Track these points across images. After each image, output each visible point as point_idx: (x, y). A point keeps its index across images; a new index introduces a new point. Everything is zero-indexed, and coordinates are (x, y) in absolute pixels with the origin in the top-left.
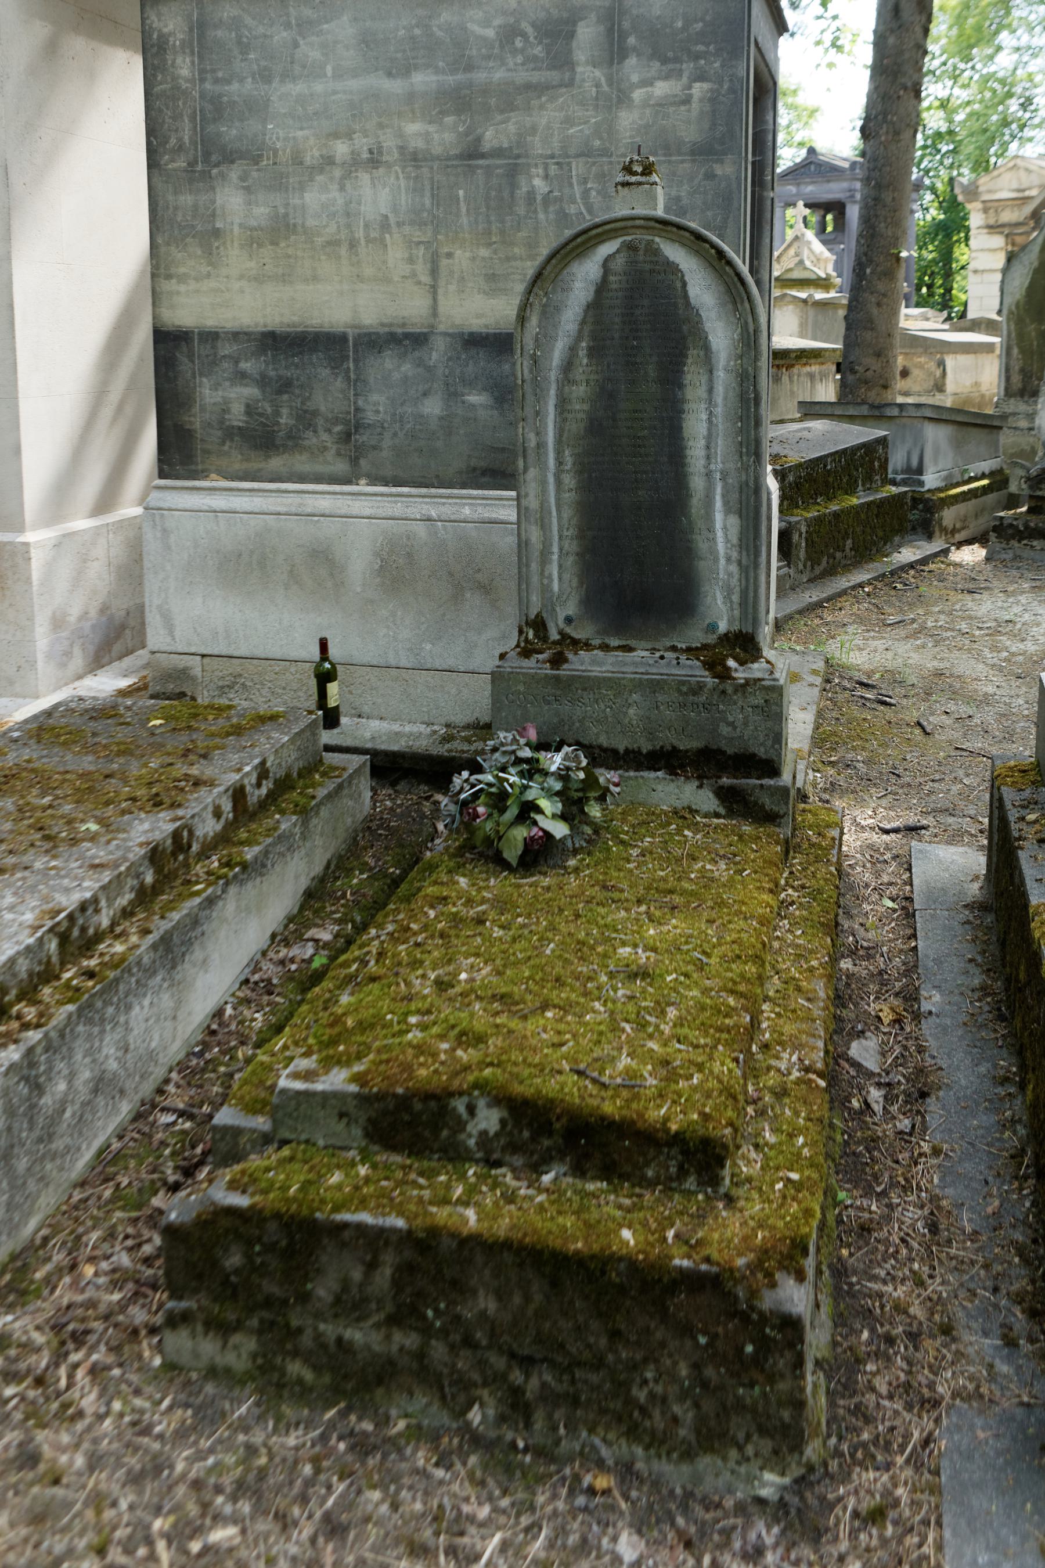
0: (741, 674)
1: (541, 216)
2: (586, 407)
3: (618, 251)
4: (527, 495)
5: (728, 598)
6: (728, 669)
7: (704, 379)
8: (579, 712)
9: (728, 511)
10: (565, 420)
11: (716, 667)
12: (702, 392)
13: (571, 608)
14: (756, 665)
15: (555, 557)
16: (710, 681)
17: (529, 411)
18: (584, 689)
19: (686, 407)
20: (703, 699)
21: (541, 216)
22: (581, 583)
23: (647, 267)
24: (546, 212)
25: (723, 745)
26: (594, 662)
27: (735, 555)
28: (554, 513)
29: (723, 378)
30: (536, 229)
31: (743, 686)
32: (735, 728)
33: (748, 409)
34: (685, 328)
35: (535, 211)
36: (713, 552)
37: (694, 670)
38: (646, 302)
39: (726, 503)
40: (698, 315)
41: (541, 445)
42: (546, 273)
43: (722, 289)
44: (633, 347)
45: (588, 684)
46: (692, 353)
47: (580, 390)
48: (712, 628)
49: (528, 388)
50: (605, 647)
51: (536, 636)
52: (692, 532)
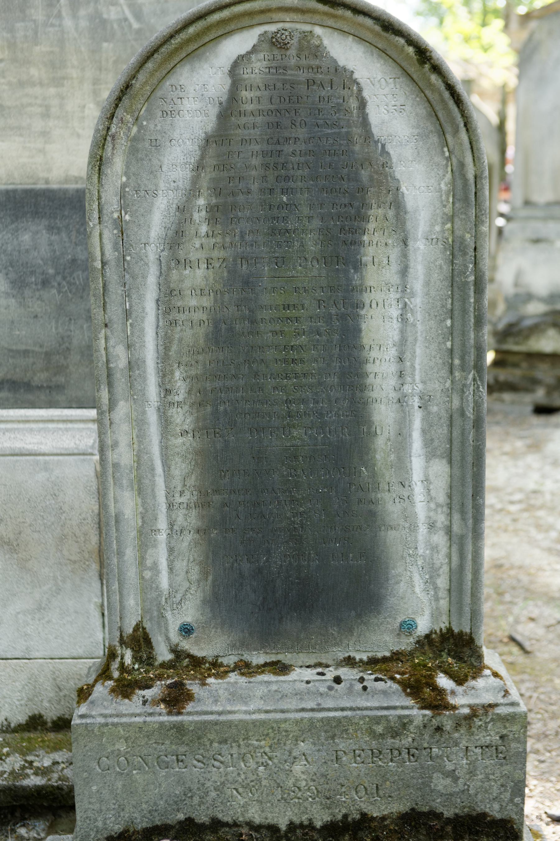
0: (462, 699)
1: (68, 23)
2: (207, 302)
3: (255, 49)
4: (115, 444)
5: (431, 582)
6: (440, 692)
7: (394, 253)
8: (215, 775)
9: (431, 454)
10: (173, 323)
11: (419, 688)
12: (391, 274)
13: (190, 613)
14: (480, 683)
15: (162, 537)
16: (418, 714)
17: (115, 312)
18: (224, 741)
19: (366, 298)
20: (407, 741)
21: (68, 23)
22: (205, 574)
23: (303, 76)
24: (75, 16)
25: (438, 805)
26: (234, 696)
27: (441, 519)
28: (159, 469)
29: (425, 255)
30: (61, 42)
31: (469, 718)
32: (456, 779)
33: (464, 300)
34: (364, 174)
35: (59, 16)
36: (409, 517)
37: (389, 698)
38: (301, 133)
39: (428, 443)
40: (384, 152)
41: (133, 365)
42: (137, 84)
43: (422, 110)
44: (281, 206)
45: (230, 733)
46: (376, 212)
47: (197, 276)
48: (407, 627)
49: (112, 274)
50: (245, 668)
51: (136, 658)
52: (377, 488)
